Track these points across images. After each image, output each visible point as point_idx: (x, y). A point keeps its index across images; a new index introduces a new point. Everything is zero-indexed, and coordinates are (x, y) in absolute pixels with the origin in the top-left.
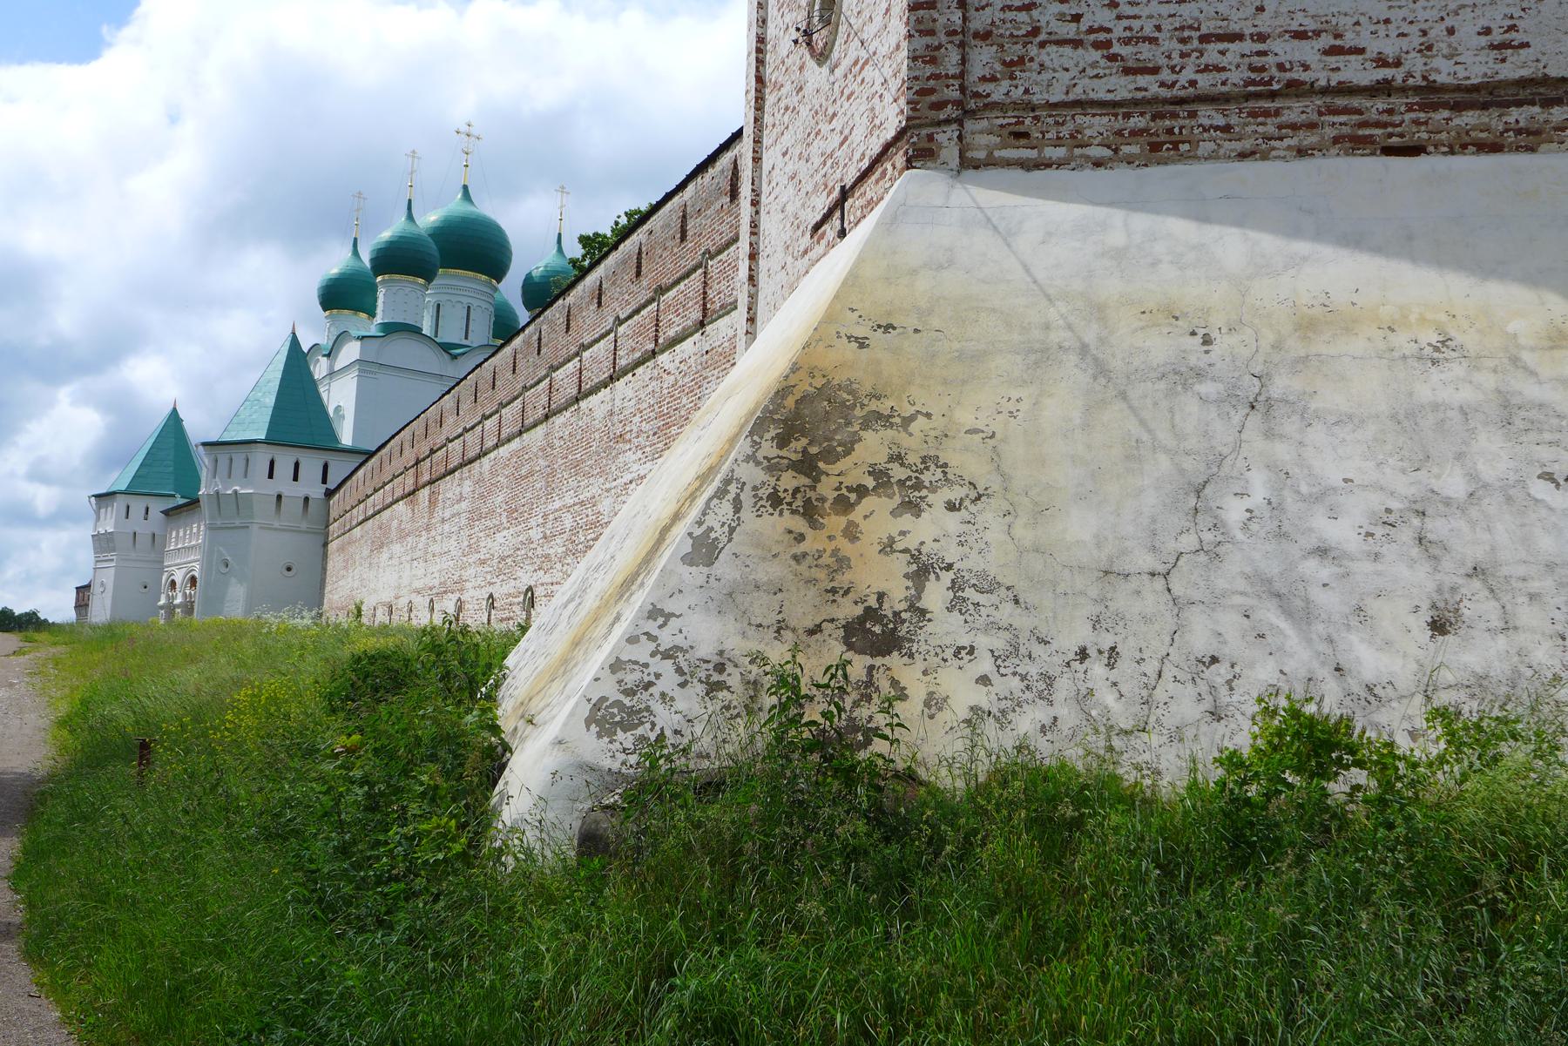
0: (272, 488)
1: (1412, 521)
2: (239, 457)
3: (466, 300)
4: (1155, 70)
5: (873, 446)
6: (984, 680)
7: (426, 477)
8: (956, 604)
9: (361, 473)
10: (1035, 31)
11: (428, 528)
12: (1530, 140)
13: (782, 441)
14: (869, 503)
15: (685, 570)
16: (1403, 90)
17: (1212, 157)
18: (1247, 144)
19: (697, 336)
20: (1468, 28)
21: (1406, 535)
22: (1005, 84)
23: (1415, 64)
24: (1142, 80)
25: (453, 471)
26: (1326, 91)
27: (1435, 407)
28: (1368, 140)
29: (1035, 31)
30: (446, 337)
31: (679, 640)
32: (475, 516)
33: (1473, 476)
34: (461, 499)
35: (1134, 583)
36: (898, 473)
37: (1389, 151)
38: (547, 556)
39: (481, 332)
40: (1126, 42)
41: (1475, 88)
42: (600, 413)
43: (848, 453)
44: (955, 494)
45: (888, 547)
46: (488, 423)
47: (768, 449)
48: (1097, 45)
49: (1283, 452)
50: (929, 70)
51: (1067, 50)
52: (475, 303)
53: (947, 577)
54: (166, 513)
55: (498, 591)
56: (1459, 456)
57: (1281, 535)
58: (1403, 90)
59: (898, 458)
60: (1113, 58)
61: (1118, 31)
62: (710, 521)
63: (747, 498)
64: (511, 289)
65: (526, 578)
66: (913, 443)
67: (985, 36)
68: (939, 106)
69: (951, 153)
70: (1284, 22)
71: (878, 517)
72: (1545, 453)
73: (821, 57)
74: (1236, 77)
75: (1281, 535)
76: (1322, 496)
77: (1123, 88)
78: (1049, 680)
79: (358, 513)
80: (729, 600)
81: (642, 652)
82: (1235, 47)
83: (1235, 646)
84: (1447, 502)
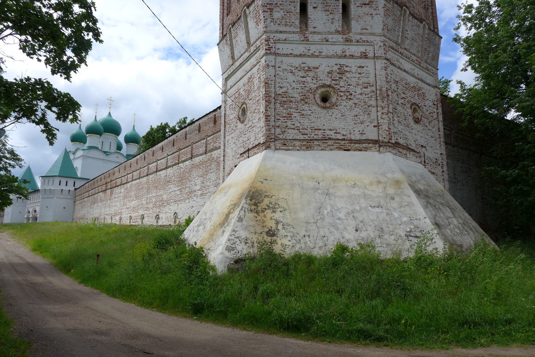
1: (352, 214)
2: (51, 180)
3: (110, 141)
4: (307, 134)
5: (266, 201)
6: (290, 241)
7: (109, 187)
8: (284, 228)
9: (87, 185)
10: (287, 126)
11: (110, 199)
12: (366, 149)
13: (251, 200)
14: (267, 211)
15: (238, 223)
16: (347, 140)
17: (317, 150)
18: (322, 148)
19: (190, 161)
20: (356, 131)
21: (351, 216)
22: (282, 135)
23: (348, 136)
24: (305, 136)
25: (118, 186)
26: (334, 140)
27: (354, 195)
28: (341, 148)
29: (287, 126)
30: (104, 150)
31: (239, 235)
32: (125, 197)
33: (360, 206)
34: (121, 193)
35: (311, 224)
36: (271, 206)
37: (345, 150)
38: (148, 208)
39: (114, 149)
40: (302, 129)
41: (358, 140)
42: (163, 175)
43: (262, 202)
44: (281, 209)
45: (271, 219)
46: (129, 175)
47: (249, 202)
48: (297, 130)
49: (332, 202)
50: (269, 132)
51: (292, 130)
52: (112, 141)
53: (282, 224)
55: (132, 215)
56: (358, 203)
57: (333, 216)
58: (347, 140)
59: (271, 203)
60: (300, 132)
61: (301, 127)
62: (241, 214)
63: (246, 210)
64: (121, 138)
65: (141, 212)
66: (273, 200)
67: (279, 127)
68: (271, 139)
69: (273, 147)
70: (328, 128)
71: (268, 213)
72: (370, 203)
73: (242, 122)
74: (320, 136)
75: (333, 216)
76: (338, 210)
77: (302, 137)
78: (300, 240)
79: (86, 195)
80: (246, 228)
81: (233, 237)
82: (320, 131)
83: (327, 234)
84: (357, 210)
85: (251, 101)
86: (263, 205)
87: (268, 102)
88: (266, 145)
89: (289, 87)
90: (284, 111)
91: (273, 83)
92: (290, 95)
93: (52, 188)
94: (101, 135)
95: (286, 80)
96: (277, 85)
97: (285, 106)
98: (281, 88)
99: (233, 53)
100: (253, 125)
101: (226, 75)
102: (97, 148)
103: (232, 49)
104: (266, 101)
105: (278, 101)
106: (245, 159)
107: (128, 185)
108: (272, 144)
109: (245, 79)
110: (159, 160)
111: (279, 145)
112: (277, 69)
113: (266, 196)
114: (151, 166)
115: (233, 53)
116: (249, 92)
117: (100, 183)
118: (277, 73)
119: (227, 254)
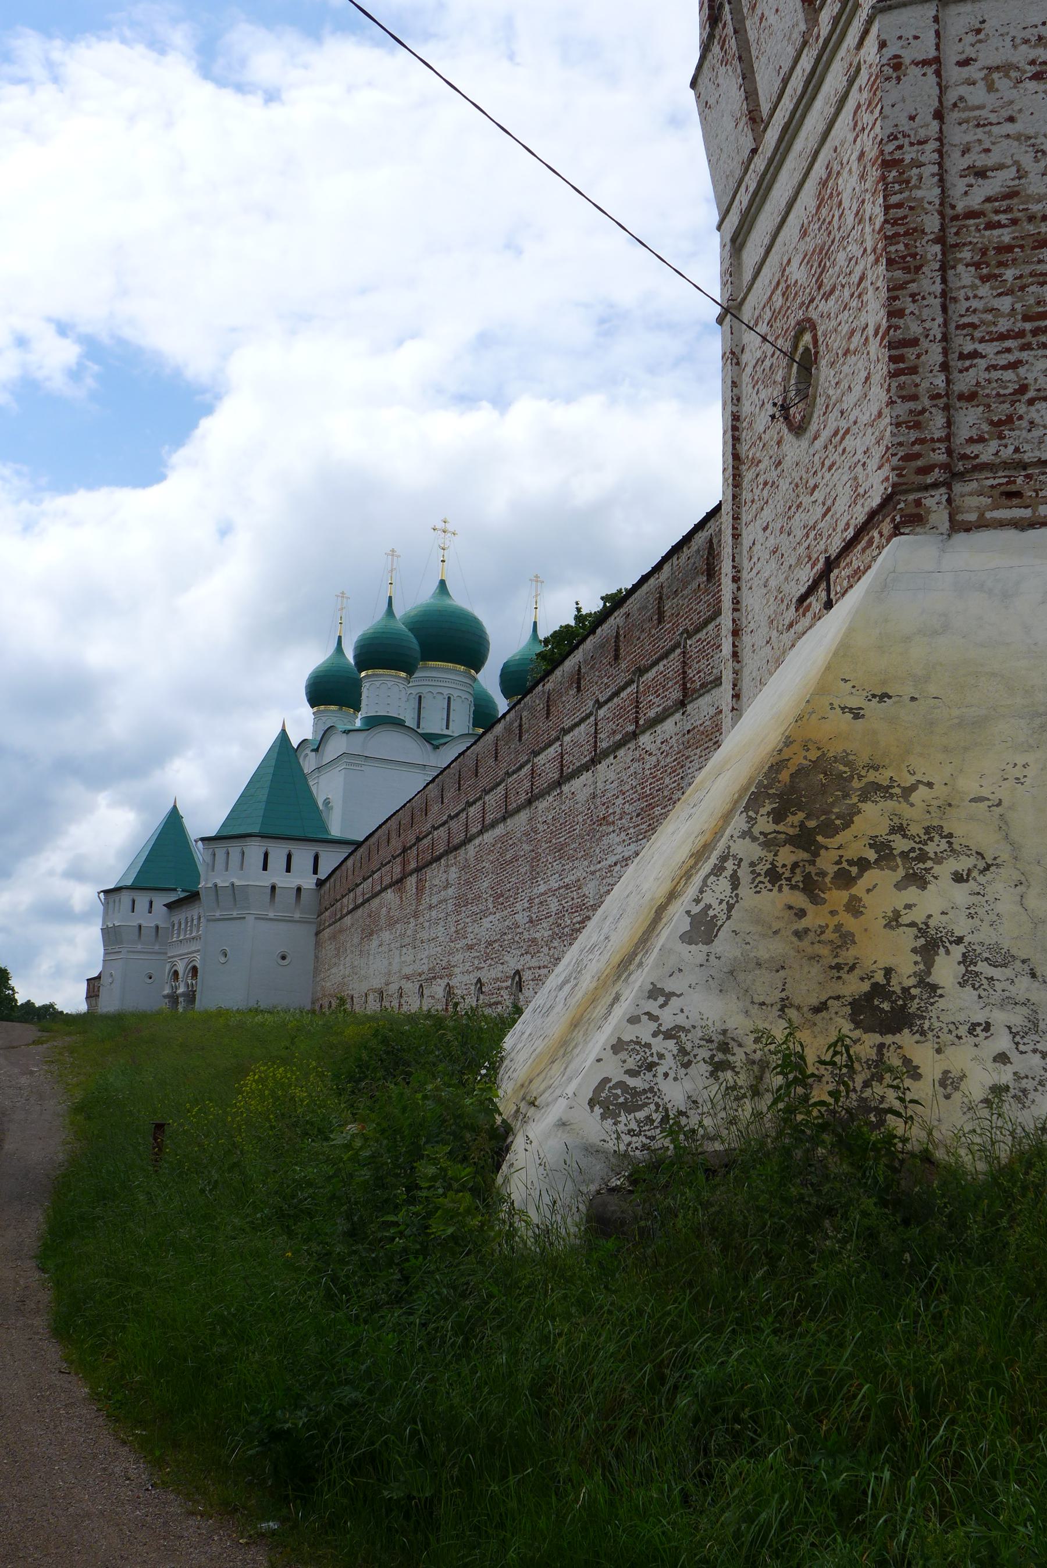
0: (266, 880)
3: (446, 691)
5: (873, 818)
7: (413, 865)
8: (970, 978)
9: (350, 862)
10: (1023, 389)
11: (416, 915)
13: (778, 816)
15: (684, 949)
19: (678, 716)
22: (994, 445)
25: (438, 859)
29: (1023, 389)
31: (681, 1020)
32: (462, 902)
36: (901, 844)
42: (582, 796)
43: (847, 824)
44: (962, 864)
45: (894, 921)
47: (764, 824)
50: (913, 435)
52: (456, 694)
53: (957, 951)
54: (169, 906)
55: (486, 976)
59: (899, 829)
62: (708, 898)
63: (744, 874)
64: (489, 678)
65: (513, 962)
66: (915, 813)
69: (940, 517)
71: (881, 891)
73: (798, 429)
79: (348, 902)
80: (730, 978)
81: (644, 1031)
85: (831, 302)
86: (852, 842)
87: (902, 265)
88: (898, 512)
89: (1027, 160)
90: (1005, 303)
91: (929, 153)
92: (1035, 208)
93: (237, 883)
94: (410, 671)
95: (1009, 128)
96: (957, 163)
97: (1009, 274)
98: (981, 173)
99: (751, 95)
100: (844, 424)
101: (734, 219)
102: (397, 723)
103: (748, 77)
104: (890, 262)
105: (966, 254)
106: (817, 618)
107: (471, 849)
108: (934, 501)
109: (808, 198)
110: (566, 731)
111: (974, 501)
112: (954, 73)
113: (884, 790)
114: (541, 759)
115: (751, 95)
116: (820, 258)
117: (385, 853)
118: (951, 96)
119: (594, 1127)
